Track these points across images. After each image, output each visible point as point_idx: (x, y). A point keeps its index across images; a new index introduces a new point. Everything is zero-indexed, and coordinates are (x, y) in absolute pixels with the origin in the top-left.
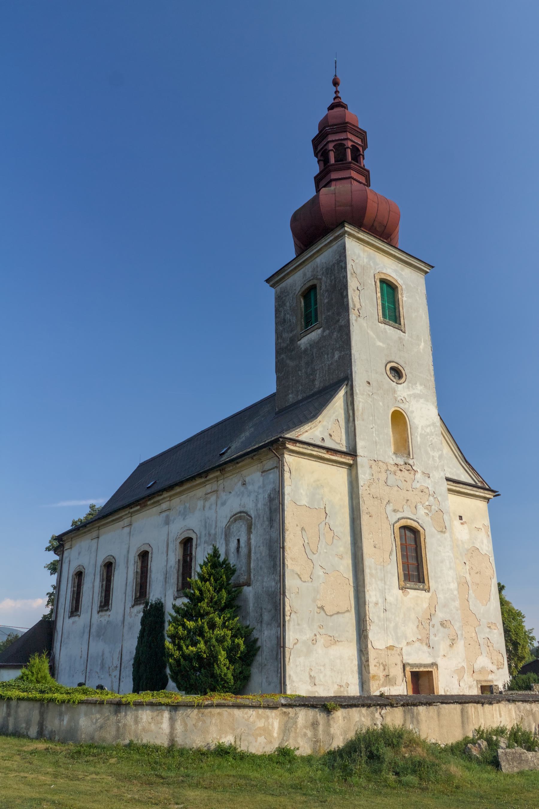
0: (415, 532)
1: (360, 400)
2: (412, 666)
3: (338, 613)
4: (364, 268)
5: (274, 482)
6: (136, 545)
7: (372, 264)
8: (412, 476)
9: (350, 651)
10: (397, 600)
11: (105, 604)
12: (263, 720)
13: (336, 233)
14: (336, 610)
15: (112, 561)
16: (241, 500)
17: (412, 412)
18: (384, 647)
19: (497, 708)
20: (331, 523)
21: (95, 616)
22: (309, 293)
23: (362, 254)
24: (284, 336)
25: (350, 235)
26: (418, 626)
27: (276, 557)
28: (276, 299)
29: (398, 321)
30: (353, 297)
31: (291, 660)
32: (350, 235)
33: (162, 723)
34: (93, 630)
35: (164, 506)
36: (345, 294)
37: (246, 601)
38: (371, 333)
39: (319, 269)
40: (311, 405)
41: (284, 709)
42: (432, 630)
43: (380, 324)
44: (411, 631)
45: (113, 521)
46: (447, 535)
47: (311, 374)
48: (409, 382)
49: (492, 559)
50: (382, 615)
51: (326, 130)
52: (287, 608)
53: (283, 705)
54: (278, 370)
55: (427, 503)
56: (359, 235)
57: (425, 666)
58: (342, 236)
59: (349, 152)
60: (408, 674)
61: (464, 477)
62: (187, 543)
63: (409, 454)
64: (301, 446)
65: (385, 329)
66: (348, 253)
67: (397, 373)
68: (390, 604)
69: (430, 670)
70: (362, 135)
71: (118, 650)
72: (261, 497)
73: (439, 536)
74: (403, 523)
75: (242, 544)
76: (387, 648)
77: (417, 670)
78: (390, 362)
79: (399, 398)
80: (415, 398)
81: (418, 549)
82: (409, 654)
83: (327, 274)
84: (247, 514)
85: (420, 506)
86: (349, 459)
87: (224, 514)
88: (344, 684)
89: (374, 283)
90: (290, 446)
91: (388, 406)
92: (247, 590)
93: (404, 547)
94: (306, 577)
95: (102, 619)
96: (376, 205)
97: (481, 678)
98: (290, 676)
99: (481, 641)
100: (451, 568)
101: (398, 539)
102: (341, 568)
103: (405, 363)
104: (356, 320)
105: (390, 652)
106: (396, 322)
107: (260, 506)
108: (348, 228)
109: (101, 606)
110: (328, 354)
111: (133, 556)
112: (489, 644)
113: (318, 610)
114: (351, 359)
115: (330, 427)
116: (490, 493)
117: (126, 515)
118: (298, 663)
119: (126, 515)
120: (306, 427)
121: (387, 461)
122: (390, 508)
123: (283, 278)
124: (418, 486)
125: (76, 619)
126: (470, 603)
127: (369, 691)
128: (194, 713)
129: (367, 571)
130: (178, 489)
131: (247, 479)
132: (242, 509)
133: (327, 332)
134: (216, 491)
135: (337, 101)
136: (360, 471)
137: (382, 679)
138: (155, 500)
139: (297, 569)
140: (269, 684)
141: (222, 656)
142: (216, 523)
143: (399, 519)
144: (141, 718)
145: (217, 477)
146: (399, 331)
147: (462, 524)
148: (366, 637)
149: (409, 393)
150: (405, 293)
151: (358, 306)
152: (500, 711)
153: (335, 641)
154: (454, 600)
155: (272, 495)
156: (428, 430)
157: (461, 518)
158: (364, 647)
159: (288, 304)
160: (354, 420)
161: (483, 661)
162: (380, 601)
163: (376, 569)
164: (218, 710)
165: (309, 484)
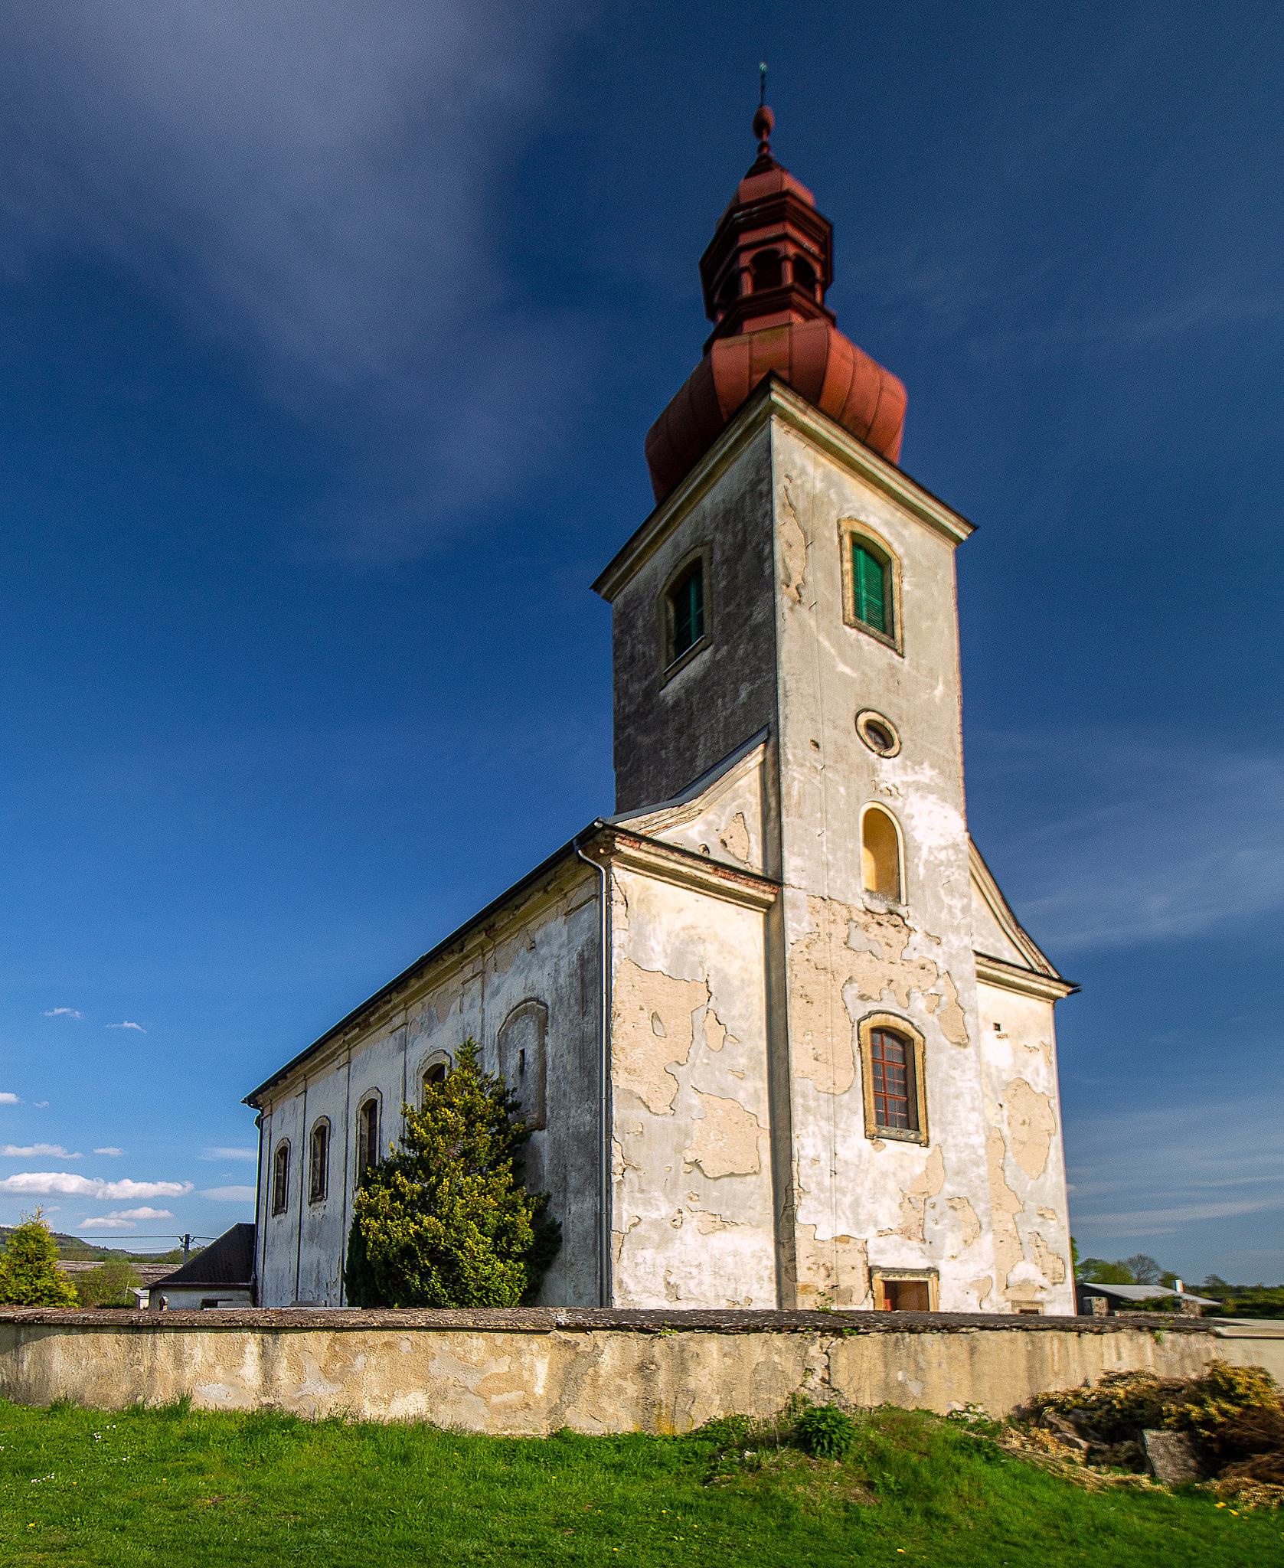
0: (904, 1041)
1: (795, 775)
2: (887, 1271)
3: (732, 1174)
5: (589, 928)
7: (834, 496)
8: (903, 936)
10: (860, 1156)
11: (318, 1193)
12: (507, 1359)
16: (526, 978)
18: (828, 1237)
19: (1113, 1343)
20: (721, 1012)
21: (306, 1208)
22: (686, 584)
23: (810, 469)
24: (631, 690)
25: (786, 418)
26: (901, 1206)
27: (593, 1068)
29: (889, 630)
30: (787, 560)
31: (624, 1255)
32: (786, 418)
33: (241, 1365)
35: (398, 1021)
36: (767, 551)
37: (536, 1155)
38: (826, 644)
39: (708, 521)
42: (930, 1212)
43: (847, 628)
44: (888, 1212)
45: (323, 1061)
46: (970, 1050)
47: (688, 749)
48: (906, 758)
49: (1055, 1102)
50: (827, 1181)
52: (617, 1159)
54: (619, 761)
55: (932, 990)
56: (805, 420)
58: (763, 421)
59: (788, 269)
60: (879, 1285)
61: (1010, 955)
64: (653, 850)
65: (858, 640)
66: (778, 458)
67: (881, 735)
68: (846, 1163)
69: (922, 1279)
72: (564, 963)
73: (953, 1052)
74: (878, 1020)
75: (530, 1057)
76: (836, 1239)
77: (897, 1278)
79: (883, 786)
80: (918, 790)
81: (909, 1071)
82: (881, 1251)
83: (727, 523)
85: (916, 994)
86: (764, 892)
87: (498, 1009)
89: (836, 539)
90: (624, 847)
91: (858, 798)
92: (541, 1137)
93: (879, 1066)
94: (659, 1106)
96: (851, 368)
98: (621, 1282)
99: (1025, 1238)
100: (973, 1109)
101: (867, 1049)
102: (741, 1095)
103: (901, 719)
104: (791, 609)
105: (840, 1246)
106: (884, 632)
107: (561, 981)
108: (778, 396)
109: (314, 1195)
112: (1040, 1243)
113: (688, 1168)
115: (722, 827)
116: (1062, 987)
117: (340, 1047)
118: (640, 1260)
119: (340, 1047)
120: (665, 815)
121: (849, 902)
122: (852, 991)
123: (630, 569)
124: (915, 956)
125: (282, 1216)
126: (1007, 1173)
129: (797, 1101)
130: (415, 984)
132: (529, 995)
134: (483, 972)
136: (788, 914)
139: (641, 1090)
141: (477, 1243)
142: (483, 1030)
143: (871, 1014)
145: (481, 946)
146: (890, 652)
147: (999, 1037)
148: (792, 1218)
149: (905, 779)
151: (797, 580)
152: (1118, 1348)
154: (976, 1164)
156: (943, 856)
157: (997, 1027)
158: (786, 1236)
159: (640, 623)
160: (779, 815)
161: (1026, 1270)
162: (825, 1156)
163: (817, 1100)
164: (386, 1336)
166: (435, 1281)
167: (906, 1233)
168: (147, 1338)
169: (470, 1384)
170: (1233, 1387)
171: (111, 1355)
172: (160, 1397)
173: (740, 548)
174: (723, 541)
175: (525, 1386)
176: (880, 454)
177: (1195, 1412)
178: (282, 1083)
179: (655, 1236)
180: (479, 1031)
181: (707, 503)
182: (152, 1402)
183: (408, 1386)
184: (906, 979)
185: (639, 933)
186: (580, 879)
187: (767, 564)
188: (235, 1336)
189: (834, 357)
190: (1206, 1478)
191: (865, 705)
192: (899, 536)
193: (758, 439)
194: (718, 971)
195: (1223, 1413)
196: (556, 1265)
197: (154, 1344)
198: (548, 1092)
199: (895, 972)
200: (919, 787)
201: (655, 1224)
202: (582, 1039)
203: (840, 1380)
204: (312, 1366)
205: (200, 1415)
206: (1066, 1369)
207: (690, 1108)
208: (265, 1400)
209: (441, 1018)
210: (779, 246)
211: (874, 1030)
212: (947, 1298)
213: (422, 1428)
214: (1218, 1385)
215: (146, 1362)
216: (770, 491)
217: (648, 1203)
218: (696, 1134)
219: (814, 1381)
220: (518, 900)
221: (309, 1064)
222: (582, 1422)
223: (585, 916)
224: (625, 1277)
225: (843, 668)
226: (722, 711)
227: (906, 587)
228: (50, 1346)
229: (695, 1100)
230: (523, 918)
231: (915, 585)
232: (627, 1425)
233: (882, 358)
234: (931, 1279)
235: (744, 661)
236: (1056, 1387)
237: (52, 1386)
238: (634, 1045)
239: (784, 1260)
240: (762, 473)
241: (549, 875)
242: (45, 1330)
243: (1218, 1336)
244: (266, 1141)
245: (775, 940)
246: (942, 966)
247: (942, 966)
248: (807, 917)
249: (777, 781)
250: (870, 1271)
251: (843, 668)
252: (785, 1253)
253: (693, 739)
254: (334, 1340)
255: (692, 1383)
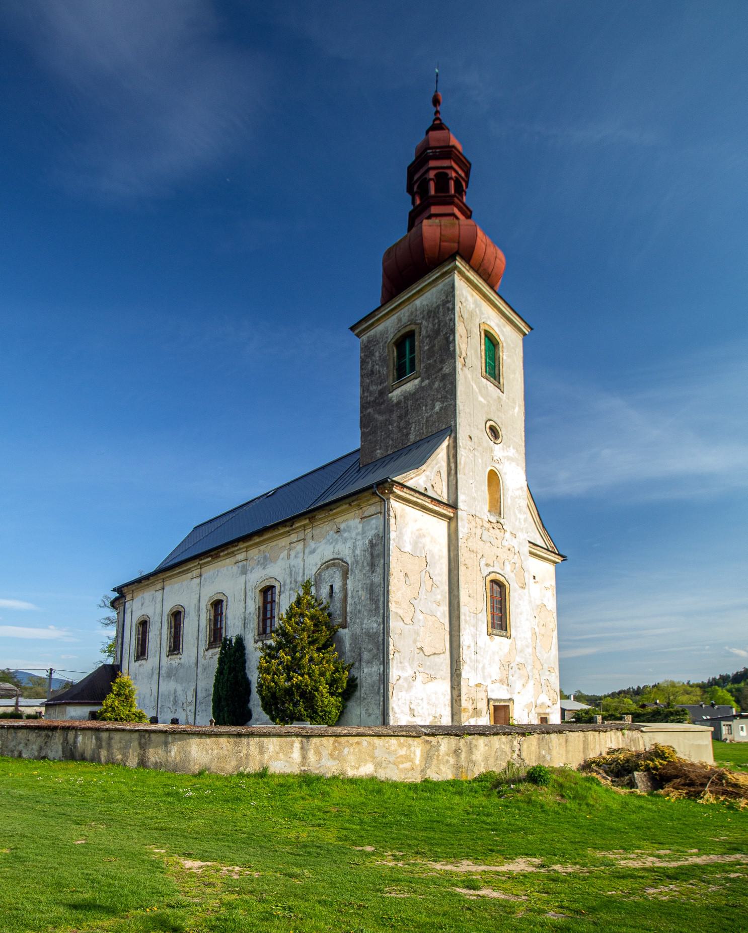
3: (435, 654)
4: (472, 314)
5: (376, 528)
6: (209, 593)
9: (445, 687)
11: (175, 647)
12: (405, 748)
13: (446, 266)
14: (434, 651)
15: (181, 609)
17: (505, 474)
19: (582, 739)
20: (431, 572)
21: (165, 659)
22: (405, 341)
24: (371, 389)
25: (461, 273)
27: (378, 600)
28: (362, 349)
32: (461, 273)
33: (292, 753)
34: (163, 671)
35: (241, 557)
36: (451, 338)
38: (475, 387)
40: (415, 452)
41: (427, 738)
44: (495, 672)
45: (179, 573)
46: (526, 590)
47: (405, 428)
51: (422, 158)
52: (391, 647)
53: (426, 735)
54: (363, 425)
57: (504, 701)
59: (452, 183)
60: (492, 708)
61: (540, 542)
62: (267, 592)
63: (500, 514)
64: (408, 492)
66: (457, 293)
67: (494, 432)
70: (466, 167)
71: (193, 688)
72: (359, 543)
74: (492, 577)
75: (337, 588)
78: (489, 420)
82: (493, 691)
83: (429, 317)
84: (342, 561)
85: (507, 563)
88: (437, 715)
90: (397, 490)
95: (173, 662)
96: (484, 246)
97: (541, 711)
99: (543, 682)
102: (439, 614)
107: (358, 552)
108: (459, 263)
110: (426, 406)
111: (205, 604)
113: (418, 651)
114: (455, 410)
120: (412, 473)
122: (483, 562)
125: (143, 662)
127: (460, 721)
128: (328, 742)
130: (257, 539)
131: (342, 526)
132: (336, 556)
133: (427, 382)
134: (304, 539)
135: (437, 122)
136: (460, 524)
137: (471, 711)
138: (229, 551)
139: (400, 612)
140: (370, 715)
141: (324, 689)
143: (490, 573)
144: (268, 749)
145: (304, 526)
148: (459, 676)
150: (505, 350)
151: (464, 355)
153: (432, 678)
154: (527, 647)
155: (374, 542)
159: (377, 354)
160: (456, 473)
162: (472, 645)
164: (357, 739)
165: (413, 532)
166: (301, 708)
167: (501, 681)
168: (244, 740)
169: (391, 760)
170: (664, 754)
171: (225, 748)
172: (253, 767)
173: (437, 332)
174: (426, 327)
175: (412, 761)
176: (492, 287)
177: (651, 764)
178: (144, 583)
179: (406, 685)
180: (301, 571)
181: (418, 302)
182: (248, 770)
183: (366, 760)
184: (503, 555)
185: (401, 533)
186: (371, 502)
187: (451, 345)
188: (289, 739)
189: (479, 240)
190: (656, 789)
191: (489, 417)
192: (502, 331)
193: (447, 280)
194: (430, 551)
195: (661, 764)
196: (354, 699)
197: (248, 743)
198: (348, 609)
199: (499, 552)
200: (509, 459)
201: (406, 679)
202: (372, 584)
203: (524, 755)
204: (325, 753)
205: (272, 776)
206: (594, 748)
207: (419, 620)
208: (303, 768)
209: (274, 560)
210: (448, 171)
211: (492, 581)
212: (520, 715)
213: (373, 779)
214: (658, 753)
215: (244, 752)
216: (454, 309)
217: (403, 669)
218: (421, 633)
219: (515, 756)
220: (332, 507)
221: (169, 574)
222: (433, 775)
223: (374, 521)
224: (394, 706)
225: (481, 399)
226: (425, 412)
227: (505, 358)
228: (189, 745)
229: (421, 617)
230: (333, 515)
231: (509, 357)
232: (450, 776)
233: (497, 243)
234: (510, 704)
235: (438, 391)
236: (592, 755)
237: (192, 763)
238: (398, 589)
239: (455, 696)
240: (449, 298)
241: (354, 498)
242: (186, 736)
243: (642, 731)
244: (128, 616)
245: (453, 536)
246: (517, 549)
247: (517, 549)
248: (467, 525)
249: (455, 456)
250: (488, 700)
251: (481, 399)
252: (456, 693)
253: (408, 424)
254: (335, 741)
255: (474, 757)
